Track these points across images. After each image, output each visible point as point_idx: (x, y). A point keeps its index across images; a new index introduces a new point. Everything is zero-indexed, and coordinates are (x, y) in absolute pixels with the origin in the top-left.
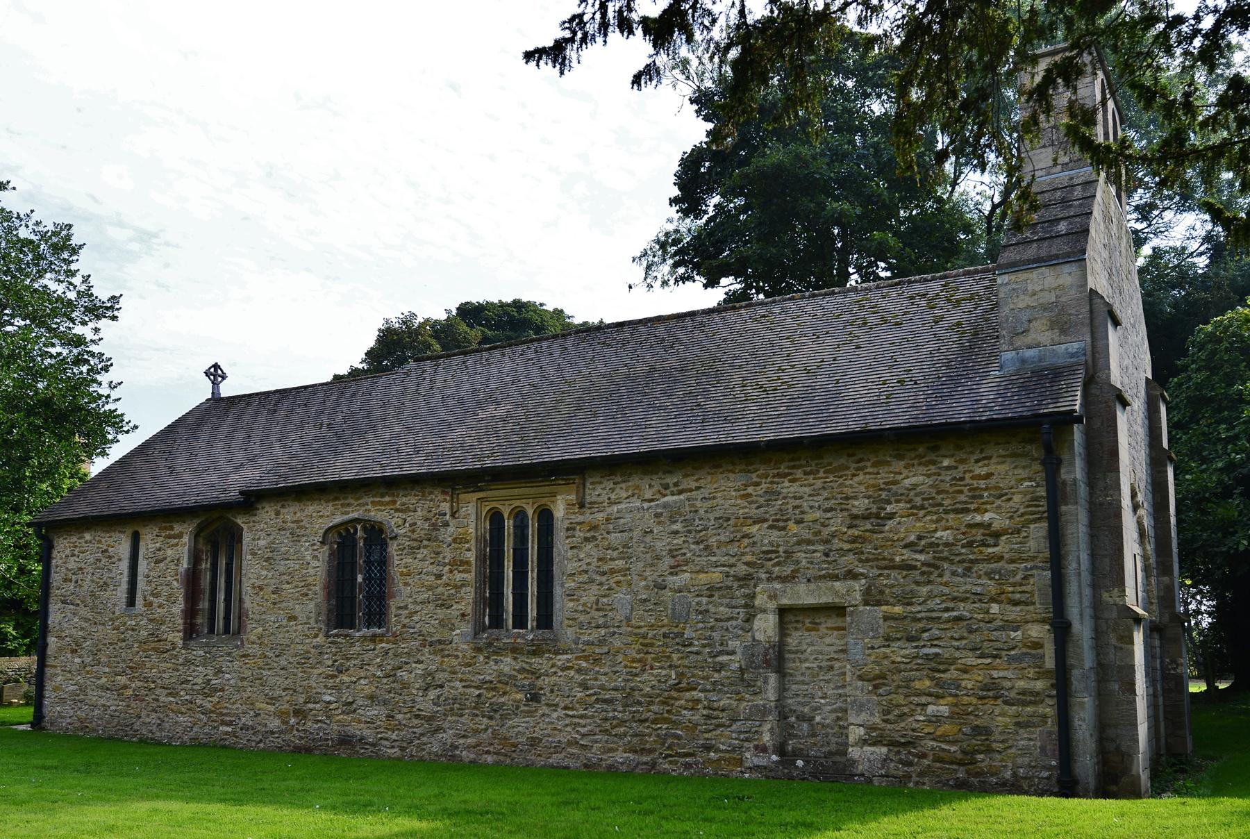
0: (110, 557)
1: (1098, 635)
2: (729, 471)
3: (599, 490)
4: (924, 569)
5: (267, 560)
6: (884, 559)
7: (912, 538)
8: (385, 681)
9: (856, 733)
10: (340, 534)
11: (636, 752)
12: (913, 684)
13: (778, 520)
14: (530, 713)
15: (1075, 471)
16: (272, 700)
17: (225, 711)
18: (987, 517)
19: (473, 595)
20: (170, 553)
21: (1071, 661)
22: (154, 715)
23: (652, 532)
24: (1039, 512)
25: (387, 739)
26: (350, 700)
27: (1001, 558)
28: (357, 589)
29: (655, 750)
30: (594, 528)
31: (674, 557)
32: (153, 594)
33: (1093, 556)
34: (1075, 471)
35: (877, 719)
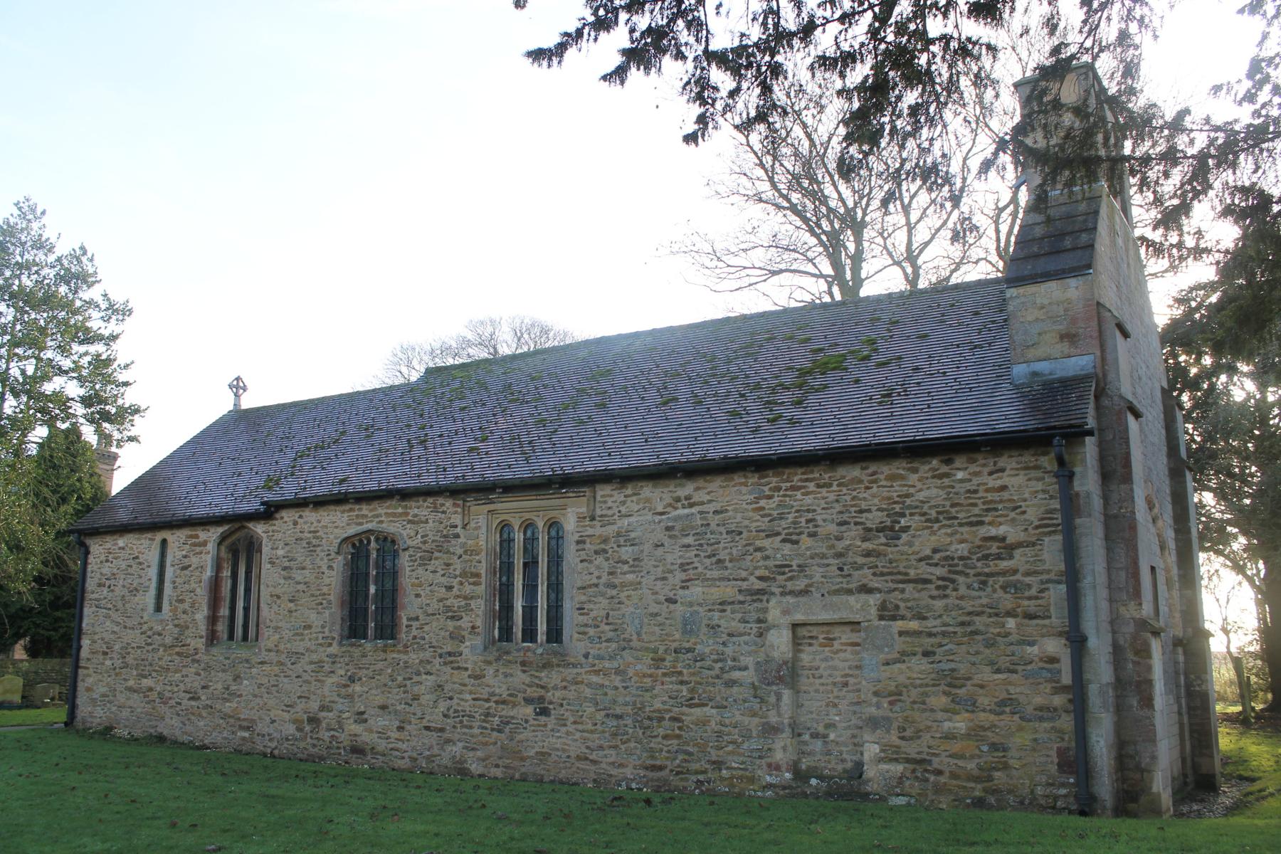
0: (140, 563)
1: (1117, 650)
2: (741, 484)
4: (940, 583)
5: (285, 569)
6: (899, 573)
7: (928, 552)
10: (354, 545)
11: (647, 768)
12: (928, 700)
13: (791, 534)
15: (1088, 481)
19: (483, 607)
20: (198, 555)
21: (1087, 676)
23: (662, 545)
24: (1053, 525)
25: (397, 750)
26: (362, 709)
27: (1015, 572)
28: (369, 603)
29: (666, 767)
30: (605, 541)
31: (685, 571)
33: (1109, 569)
34: (1088, 481)
35: (894, 739)
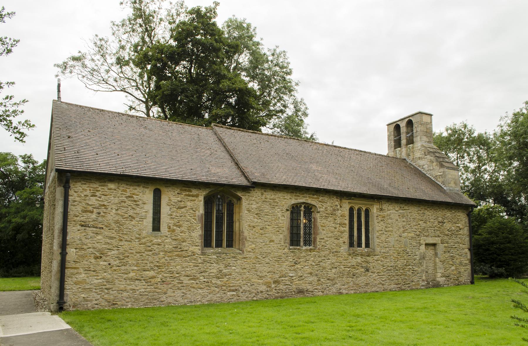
3: (385, 206)
5: (257, 214)
8: (316, 266)
9: (439, 275)
14: (365, 275)
16: (261, 277)
17: (231, 285)
18: (459, 225)
22: (179, 291)
26: (302, 275)
30: (384, 217)
32: (175, 225)
